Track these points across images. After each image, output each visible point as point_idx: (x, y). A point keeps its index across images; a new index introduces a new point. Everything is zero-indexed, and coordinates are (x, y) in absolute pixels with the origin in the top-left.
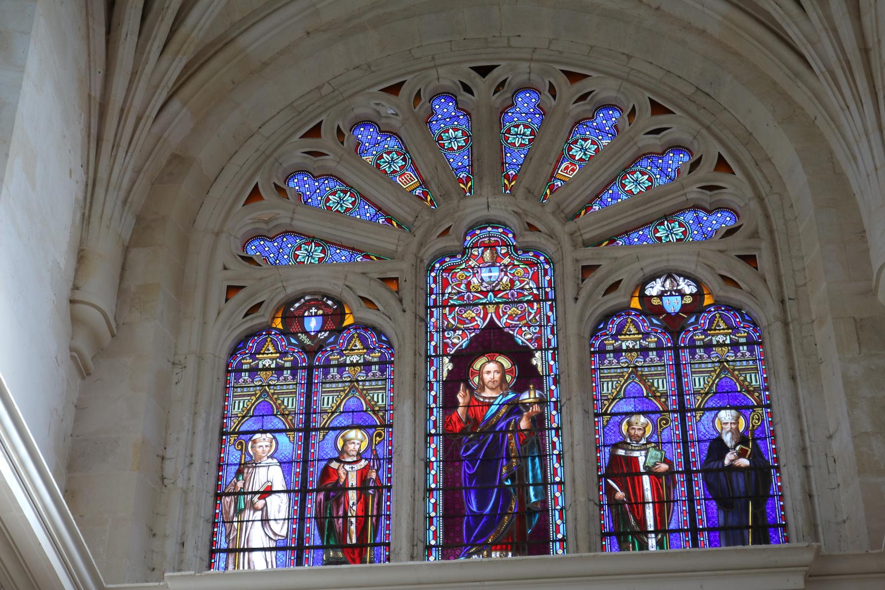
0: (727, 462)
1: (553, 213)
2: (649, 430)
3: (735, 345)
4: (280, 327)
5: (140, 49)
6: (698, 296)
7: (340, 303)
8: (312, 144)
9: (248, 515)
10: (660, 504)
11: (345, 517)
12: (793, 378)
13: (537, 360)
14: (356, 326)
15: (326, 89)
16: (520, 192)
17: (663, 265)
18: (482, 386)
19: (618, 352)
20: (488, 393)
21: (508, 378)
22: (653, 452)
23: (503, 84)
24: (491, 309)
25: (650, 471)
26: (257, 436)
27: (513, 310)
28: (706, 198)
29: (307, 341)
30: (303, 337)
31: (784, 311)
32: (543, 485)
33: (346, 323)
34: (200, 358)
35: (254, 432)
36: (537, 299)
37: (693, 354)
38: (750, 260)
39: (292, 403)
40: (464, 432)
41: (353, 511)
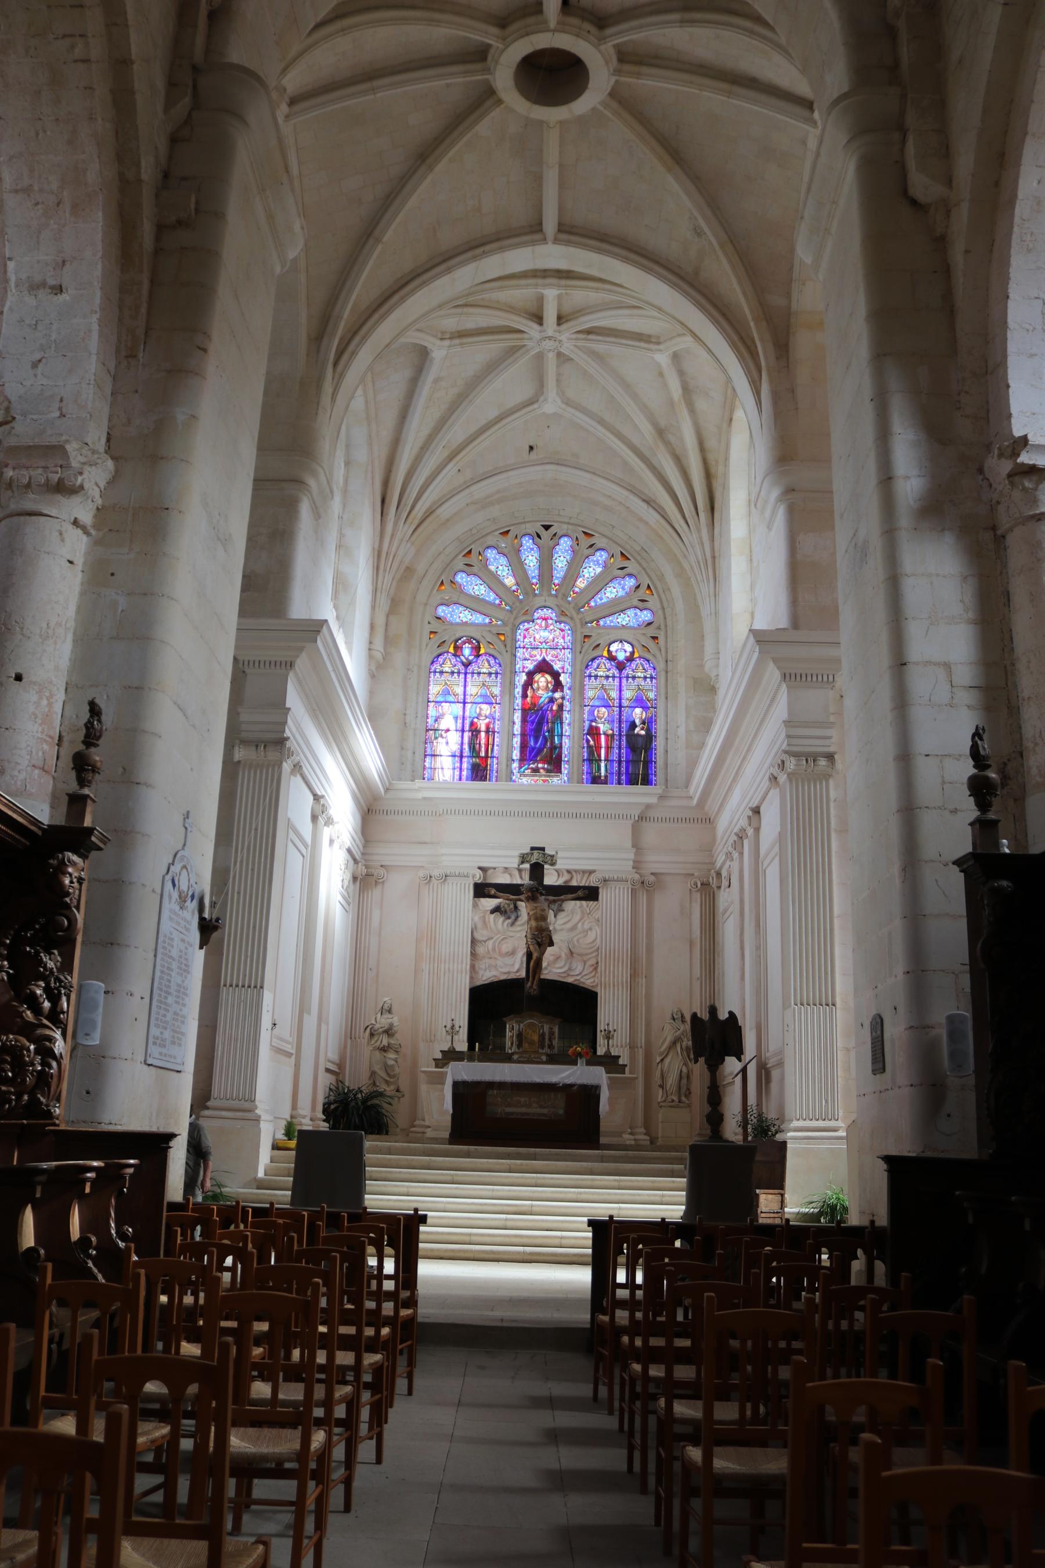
0: (636, 732)
1: (551, 943)
2: (606, 714)
3: (645, 678)
4: (452, 652)
5: (396, 524)
6: (633, 653)
7: (478, 642)
8: (467, 561)
9: (440, 739)
10: (607, 748)
11: (480, 744)
12: (667, 698)
13: (561, 678)
14: (486, 654)
15: (474, 531)
16: (560, 596)
17: (619, 638)
18: (538, 689)
19: (596, 677)
20: (540, 692)
21: (549, 685)
22: (607, 725)
23: (555, 534)
24: (544, 651)
25: (605, 734)
26: (443, 704)
27: (553, 652)
28: (641, 605)
29: (464, 660)
30: (462, 657)
31: (667, 665)
32: (561, 736)
33: (481, 653)
34: (419, 667)
35: (442, 702)
36: (564, 648)
37: (627, 680)
38: (655, 638)
39: (459, 690)
40: (530, 709)
41: (483, 742)
